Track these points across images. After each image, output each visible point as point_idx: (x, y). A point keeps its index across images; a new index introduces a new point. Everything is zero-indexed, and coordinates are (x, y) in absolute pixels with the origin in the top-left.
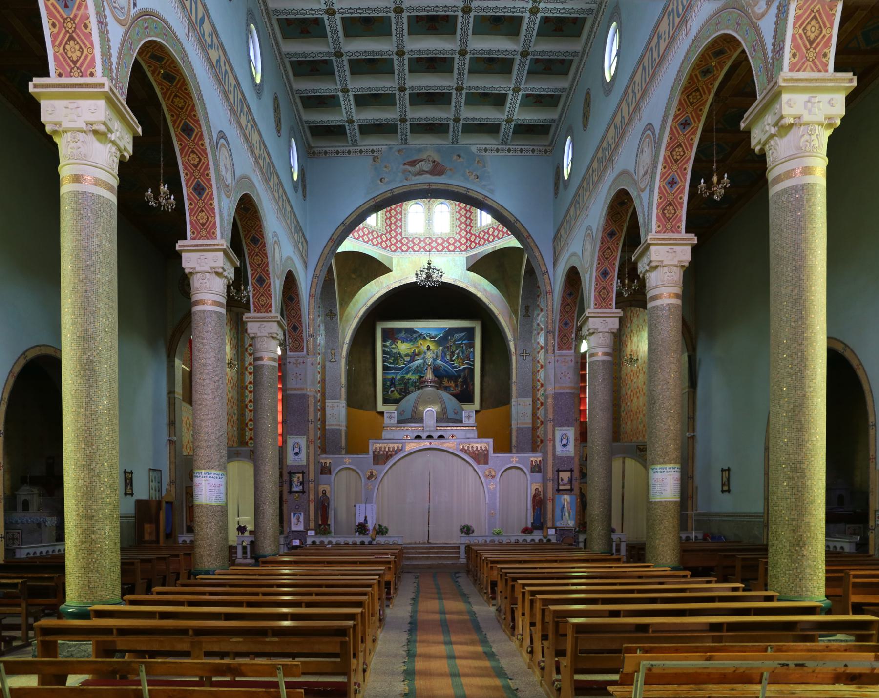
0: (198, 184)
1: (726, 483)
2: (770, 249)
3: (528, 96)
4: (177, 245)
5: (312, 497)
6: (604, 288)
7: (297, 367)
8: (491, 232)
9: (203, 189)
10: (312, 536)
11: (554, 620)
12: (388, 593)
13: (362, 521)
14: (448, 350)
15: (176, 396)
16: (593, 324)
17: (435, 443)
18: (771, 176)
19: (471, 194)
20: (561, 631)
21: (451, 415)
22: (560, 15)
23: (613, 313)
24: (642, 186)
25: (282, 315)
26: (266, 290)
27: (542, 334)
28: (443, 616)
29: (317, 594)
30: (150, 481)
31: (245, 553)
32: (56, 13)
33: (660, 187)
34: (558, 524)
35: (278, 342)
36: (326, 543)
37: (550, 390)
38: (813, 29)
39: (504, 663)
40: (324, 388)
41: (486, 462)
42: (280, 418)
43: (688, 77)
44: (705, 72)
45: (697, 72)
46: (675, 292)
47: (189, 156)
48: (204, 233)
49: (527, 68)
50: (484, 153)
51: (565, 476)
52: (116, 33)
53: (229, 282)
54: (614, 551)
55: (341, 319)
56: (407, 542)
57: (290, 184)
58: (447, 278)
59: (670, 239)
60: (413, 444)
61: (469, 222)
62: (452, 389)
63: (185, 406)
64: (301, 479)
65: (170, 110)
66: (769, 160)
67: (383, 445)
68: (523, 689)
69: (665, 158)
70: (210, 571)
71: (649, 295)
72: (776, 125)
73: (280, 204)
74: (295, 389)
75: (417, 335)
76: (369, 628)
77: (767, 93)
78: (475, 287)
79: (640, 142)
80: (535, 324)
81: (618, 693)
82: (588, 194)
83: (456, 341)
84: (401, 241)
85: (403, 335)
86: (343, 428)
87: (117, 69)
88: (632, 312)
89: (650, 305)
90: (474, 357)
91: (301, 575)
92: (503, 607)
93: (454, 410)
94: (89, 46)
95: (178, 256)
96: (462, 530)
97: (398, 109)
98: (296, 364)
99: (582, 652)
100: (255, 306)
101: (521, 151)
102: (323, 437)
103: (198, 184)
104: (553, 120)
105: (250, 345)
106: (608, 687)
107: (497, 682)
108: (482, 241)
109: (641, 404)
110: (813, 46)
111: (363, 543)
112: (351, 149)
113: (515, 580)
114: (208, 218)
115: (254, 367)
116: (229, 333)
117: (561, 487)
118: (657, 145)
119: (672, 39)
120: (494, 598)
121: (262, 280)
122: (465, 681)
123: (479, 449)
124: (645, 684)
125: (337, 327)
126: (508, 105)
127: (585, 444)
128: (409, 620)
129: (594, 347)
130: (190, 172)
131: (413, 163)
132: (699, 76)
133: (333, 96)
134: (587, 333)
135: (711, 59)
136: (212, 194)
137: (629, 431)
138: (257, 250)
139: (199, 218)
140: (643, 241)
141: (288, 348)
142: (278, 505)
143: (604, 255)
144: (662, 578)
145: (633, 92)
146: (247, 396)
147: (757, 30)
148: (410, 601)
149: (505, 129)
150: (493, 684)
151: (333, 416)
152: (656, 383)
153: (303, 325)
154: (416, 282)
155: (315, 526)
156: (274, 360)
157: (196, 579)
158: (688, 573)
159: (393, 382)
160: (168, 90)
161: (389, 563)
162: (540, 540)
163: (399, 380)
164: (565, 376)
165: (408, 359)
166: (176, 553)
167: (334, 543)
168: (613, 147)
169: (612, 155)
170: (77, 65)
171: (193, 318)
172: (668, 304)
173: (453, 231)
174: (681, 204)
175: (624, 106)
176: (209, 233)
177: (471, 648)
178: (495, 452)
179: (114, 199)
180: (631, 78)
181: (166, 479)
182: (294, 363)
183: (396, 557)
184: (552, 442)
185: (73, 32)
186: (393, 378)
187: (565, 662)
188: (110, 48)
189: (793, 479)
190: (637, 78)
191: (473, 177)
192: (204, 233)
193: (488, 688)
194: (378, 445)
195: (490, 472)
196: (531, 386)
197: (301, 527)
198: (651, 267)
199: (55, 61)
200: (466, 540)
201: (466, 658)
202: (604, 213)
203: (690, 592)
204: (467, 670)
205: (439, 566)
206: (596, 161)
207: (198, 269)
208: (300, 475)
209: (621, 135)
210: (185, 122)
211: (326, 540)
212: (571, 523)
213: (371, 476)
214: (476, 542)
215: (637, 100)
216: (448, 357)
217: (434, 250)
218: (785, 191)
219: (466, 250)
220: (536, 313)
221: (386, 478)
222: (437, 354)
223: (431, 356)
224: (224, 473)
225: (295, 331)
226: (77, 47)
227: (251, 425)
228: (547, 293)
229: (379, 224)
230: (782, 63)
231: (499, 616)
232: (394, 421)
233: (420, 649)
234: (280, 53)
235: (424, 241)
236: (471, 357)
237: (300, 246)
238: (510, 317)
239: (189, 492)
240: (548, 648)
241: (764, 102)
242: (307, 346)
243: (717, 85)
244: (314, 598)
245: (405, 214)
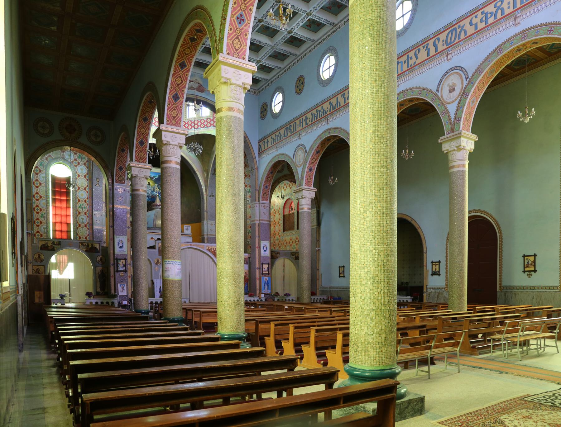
0: (176, 95)
9: (178, 98)
32: (234, 24)
48: (174, 122)
64: (124, 263)
91: (271, 316)
100: (136, 158)
103: (176, 95)
114: (177, 115)
117: (264, 273)
130: (174, 87)
138: (144, 125)
139: (172, 113)
146: (35, 203)
170: (238, 52)
176: (177, 122)
185: (239, 35)
189: (461, 273)
199: (227, 46)
208: (124, 261)
222: (154, 188)
225: (121, 170)
226: (239, 43)
238: (203, 173)
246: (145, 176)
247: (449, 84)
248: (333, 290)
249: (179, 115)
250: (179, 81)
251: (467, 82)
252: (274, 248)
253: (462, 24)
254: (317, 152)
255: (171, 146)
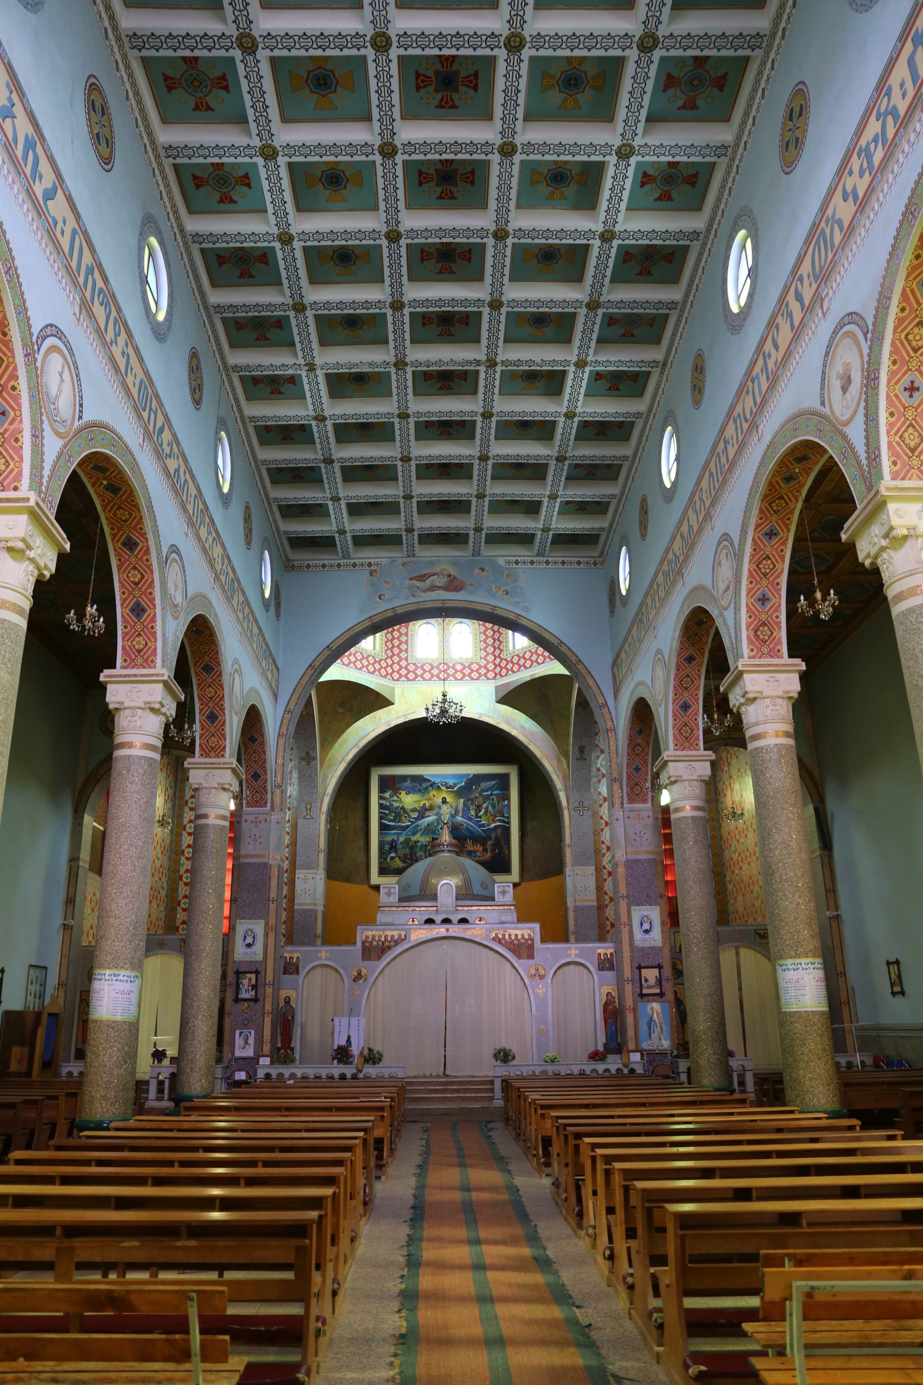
0: (138, 605)
1: (897, 982)
2: (905, 678)
3: (568, 503)
4: (102, 675)
5: (268, 1007)
6: (686, 725)
7: (256, 826)
8: (527, 655)
10: (265, 1066)
11: (643, 1206)
12: (380, 1157)
13: (343, 1042)
14: (472, 804)
15: (81, 864)
16: (673, 769)
17: (455, 930)
18: (890, 593)
19: (499, 612)
20: (657, 1223)
21: (477, 890)
22: (602, 419)
23: (702, 756)
24: (724, 603)
25: (239, 760)
26: (218, 730)
27: (604, 781)
28: (466, 1194)
29: (267, 1164)
30: (29, 982)
31: (160, 1091)
33: (747, 606)
34: (645, 1045)
35: (231, 795)
36: (287, 1076)
37: (621, 856)
38: (912, 437)
39: (567, 1277)
40: (293, 854)
41: (531, 956)
42: (227, 895)
43: (767, 483)
44: (788, 479)
45: (778, 479)
46: (784, 729)
47: (129, 572)
49: (565, 473)
50: (515, 566)
51: (651, 975)
52: (52, 446)
53: (168, 720)
54: (736, 1086)
55: (322, 763)
56: (413, 1074)
57: (260, 602)
58: (471, 712)
59: (769, 665)
60: (422, 931)
61: (498, 645)
62: (478, 854)
63: (93, 878)
64: (253, 982)
65: (110, 523)
66: (885, 575)
67: (377, 933)
68: (600, 1325)
69: (750, 572)
70: (103, 1122)
71: (748, 734)
72: (886, 536)
73: (245, 625)
74: (253, 856)
75: (429, 784)
76: (345, 1218)
77: (868, 503)
78: (508, 722)
79: (716, 554)
80: (594, 769)
81: (762, 1336)
82: (653, 612)
83: (482, 791)
84: (406, 668)
85: (408, 783)
86: (320, 909)
87: (48, 482)
88: (728, 752)
89: (751, 746)
90: (509, 812)
91: (243, 1131)
92: (562, 1180)
93: (482, 884)
94: (17, 459)
95: (103, 688)
96: (496, 1056)
97: (403, 519)
98: (256, 822)
99: (694, 1259)
101: (563, 563)
102: (291, 919)
103: (138, 605)
104: (602, 529)
105: (193, 797)
106: (744, 1325)
107: (556, 1312)
108: (516, 668)
109: (755, 872)
110: (916, 454)
111: (343, 1077)
112: (341, 562)
113: (579, 1136)
114: (146, 644)
115: (195, 827)
116: (163, 782)
117: (645, 991)
118: (739, 557)
119: (742, 446)
120: (548, 1164)
121: (214, 717)
122: (501, 1310)
123: (519, 937)
124: (806, 1318)
125: (316, 774)
126: (544, 513)
127: (677, 930)
128: (411, 1203)
129: (679, 800)
131: (422, 578)
132: (780, 483)
133: (320, 505)
134: (668, 782)
135: (792, 464)
136: (155, 616)
137: (741, 909)
138: (210, 680)
139: (134, 643)
140: (732, 668)
141: (245, 802)
142: (216, 1020)
143: (682, 684)
144: (814, 1132)
145: (701, 499)
146: (183, 865)
147: (844, 437)
148: (413, 1170)
149: (540, 542)
150: (549, 1316)
151: (305, 892)
152: (771, 846)
153: (268, 772)
154: (426, 718)
155: (271, 1051)
156: (224, 818)
157: (80, 1137)
158: (856, 1122)
159: (393, 846)
160: (109, 502)
161: (382, 1109)
162: (618, 1070)
163: (402, 843)
164: (641, 837)
165: (415, 815)
166: (53, 1092)
167: (299, 1076)
168: (681, 558)
169: (680, 568)
171: (114, 764)
172: (776, 745)
173: (476, 655)
174: (778, 624)
175: (691, 513)
176: (146, 661)
177: (512, 1251)
178: (543, 941)
179: (23, 623)
180: (696, 483)
181: (53, 979)
182: (252, 822)
183: (392, 1099)
184: (627, 927)
186: (393, 841)
187: (667, 1275)
188: (42, 461)
190: (704, 484)
191: (500, 593)
192: (139, 660)
193: (538, 1322)
194: (370, 933)
195: (537, 970)
196: (592, 851)
197: (249, 1052)
198: (748, 700)
200: (502, 1071)
201: (503, 1268)
202: (677, 634)
203: (863, 1155)
204: (505, 1291)
205: (461, 1111)
206: (661, 574)
207: (126, 704)
208: (253, 976)
209: (691, 546)
210: (128, 535)
211: (286, 1071)
212: (666, 1044)
213: (359, 976)
214: (519, 1073)
215: (707, 507)
216: (473, 813)
217: (451, 678)
218: (912, 610)
219: (494, 678)
220: (594, 755)
221: (380, 978)
222: (457, 807)
223: (447, 811)
224: (138, 974)
225: (256, 780)
227: (185, 903)
228: (607, 730)
229: (377, 648)
230: (881, 470)
231: (557, 1194)
232: (394, 899)
233: (429, 1253)
234: (255, 460)
235: (438, 667)
236: (505, 811)
237: (269, 674)
238: (559, 761)
239: (84, 999)
240: (638, 1252)
241: (866, 512)
242: (272, 800)
243: (804, 491)
244: (260, 1171)
245: (412, 635)
246: (218, 784)
247: (838, 373)
248: (885, 1037)
249: (149, 644)
250: (135, 576)
251: (869, 343)
252: (755, 919)
253: (829, 212)
254: (686, 659)
255: (127, 712)
